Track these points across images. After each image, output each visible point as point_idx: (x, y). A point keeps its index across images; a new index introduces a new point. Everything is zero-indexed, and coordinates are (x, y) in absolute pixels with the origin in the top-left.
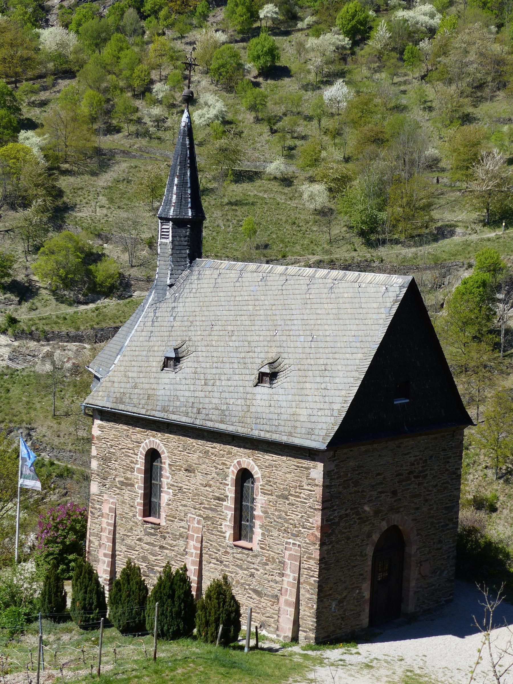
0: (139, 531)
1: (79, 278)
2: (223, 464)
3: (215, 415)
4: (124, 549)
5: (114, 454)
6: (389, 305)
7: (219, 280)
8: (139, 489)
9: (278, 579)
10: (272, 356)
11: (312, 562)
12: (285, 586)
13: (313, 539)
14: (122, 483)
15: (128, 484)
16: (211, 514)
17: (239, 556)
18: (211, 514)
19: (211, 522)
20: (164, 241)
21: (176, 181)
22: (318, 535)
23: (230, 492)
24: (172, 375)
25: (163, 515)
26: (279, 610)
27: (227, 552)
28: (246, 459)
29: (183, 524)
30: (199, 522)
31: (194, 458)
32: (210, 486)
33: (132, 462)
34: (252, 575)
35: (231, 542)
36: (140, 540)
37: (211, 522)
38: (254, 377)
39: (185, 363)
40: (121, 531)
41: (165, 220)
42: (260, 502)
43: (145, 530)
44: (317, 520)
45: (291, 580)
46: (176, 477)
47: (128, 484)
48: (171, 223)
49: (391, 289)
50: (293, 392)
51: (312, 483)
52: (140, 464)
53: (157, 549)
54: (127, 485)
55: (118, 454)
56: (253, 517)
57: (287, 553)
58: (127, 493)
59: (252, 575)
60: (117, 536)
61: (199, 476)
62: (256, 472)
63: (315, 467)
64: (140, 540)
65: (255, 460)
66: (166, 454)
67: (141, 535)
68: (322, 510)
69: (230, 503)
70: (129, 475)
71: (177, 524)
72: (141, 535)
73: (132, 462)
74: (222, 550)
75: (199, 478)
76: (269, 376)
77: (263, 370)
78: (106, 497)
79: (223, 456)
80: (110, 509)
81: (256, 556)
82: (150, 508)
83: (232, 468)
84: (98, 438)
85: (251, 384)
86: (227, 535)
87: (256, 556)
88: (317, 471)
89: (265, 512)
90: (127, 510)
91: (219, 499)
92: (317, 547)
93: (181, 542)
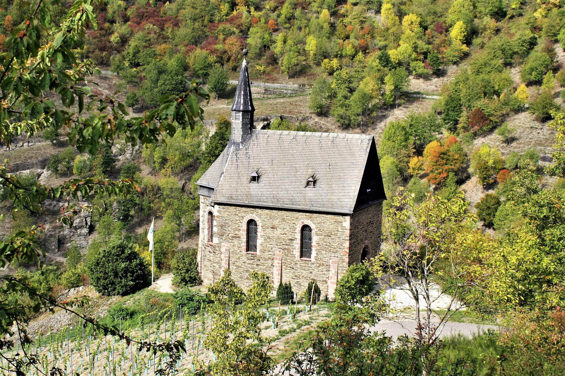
0: (244, 259)
1: (102, 140)
2: (294, 223)
3: (287, 201)
4: (235, 267)
5: (227, 223)
6: (365, 148)
7: (269, 139)
8: (244, 238)
9: (326, 273)
10: (310, 172)
11: (344, 264)
12: (330, 275)
13: (345, 253)
14: (233, 237)
15: (237, 237)
16: (286, 247)
17: (303, 265)
18: (286, 247)
19: (287, 251)
20: (237, 121)
21: (242, 93)
22: (348, 251)
23: (298, 236)
24: (257, 184)
25: (258, 249)
26: (328, 286)
27: (296, 264)
28: (305, 219)
29: (270, 253)
30: (280, 251)
31: (276, 222)
32: (286, 234)
33: (239, 226)
34: (311, 273)
35: (299, 259)
36: (244, 263)
37: (287, 251)
38: (305, 182)
39: (261, 179)
40: (233, 260)
41: (239, 111)
42: (315, 239)
43: (247, 258)
44: (347, 244)
45: (334, 272)
46: (266, 232)
47: (237, 237)
48: (241, 113)
49: (364, 141)
50: (326, 189)
51: (344, 228)
52: (244, 227)
53: (255, 266)
54: (236, 237)
55: (230, 223)
56: (311, 246)
57: (331, 261)
58: (236, 241)
59: (311, 273)
60: (230, 262)
61: (279, 230)
62: (312, 226)
63: (345, 221)
64: (244, 263)
65: (311, 221)
66: (260, 221)
67: (245, 260)
68: (350, 240)
69: (298, 241)
70: (237, 232)
71: (266, 253)
72: (245, 260)
73: (239, 226)
74: (293, 263)
75: (278, 232)
76: (313, 182)
77: (309, 180)
78: (223, 244)
79: (293, 220)
80: (226, 250)
81: (313, 264)
82: (250, 246)
83: (298, 225)
84: (217, 217)
85: (303, 186)
86: (296, 256)
87: (313, 264)
88: (347, 222)
89: (318, 244)
90: (236, 248)
91: (291, 240)
92: (347, 256)
93: (269, 261)
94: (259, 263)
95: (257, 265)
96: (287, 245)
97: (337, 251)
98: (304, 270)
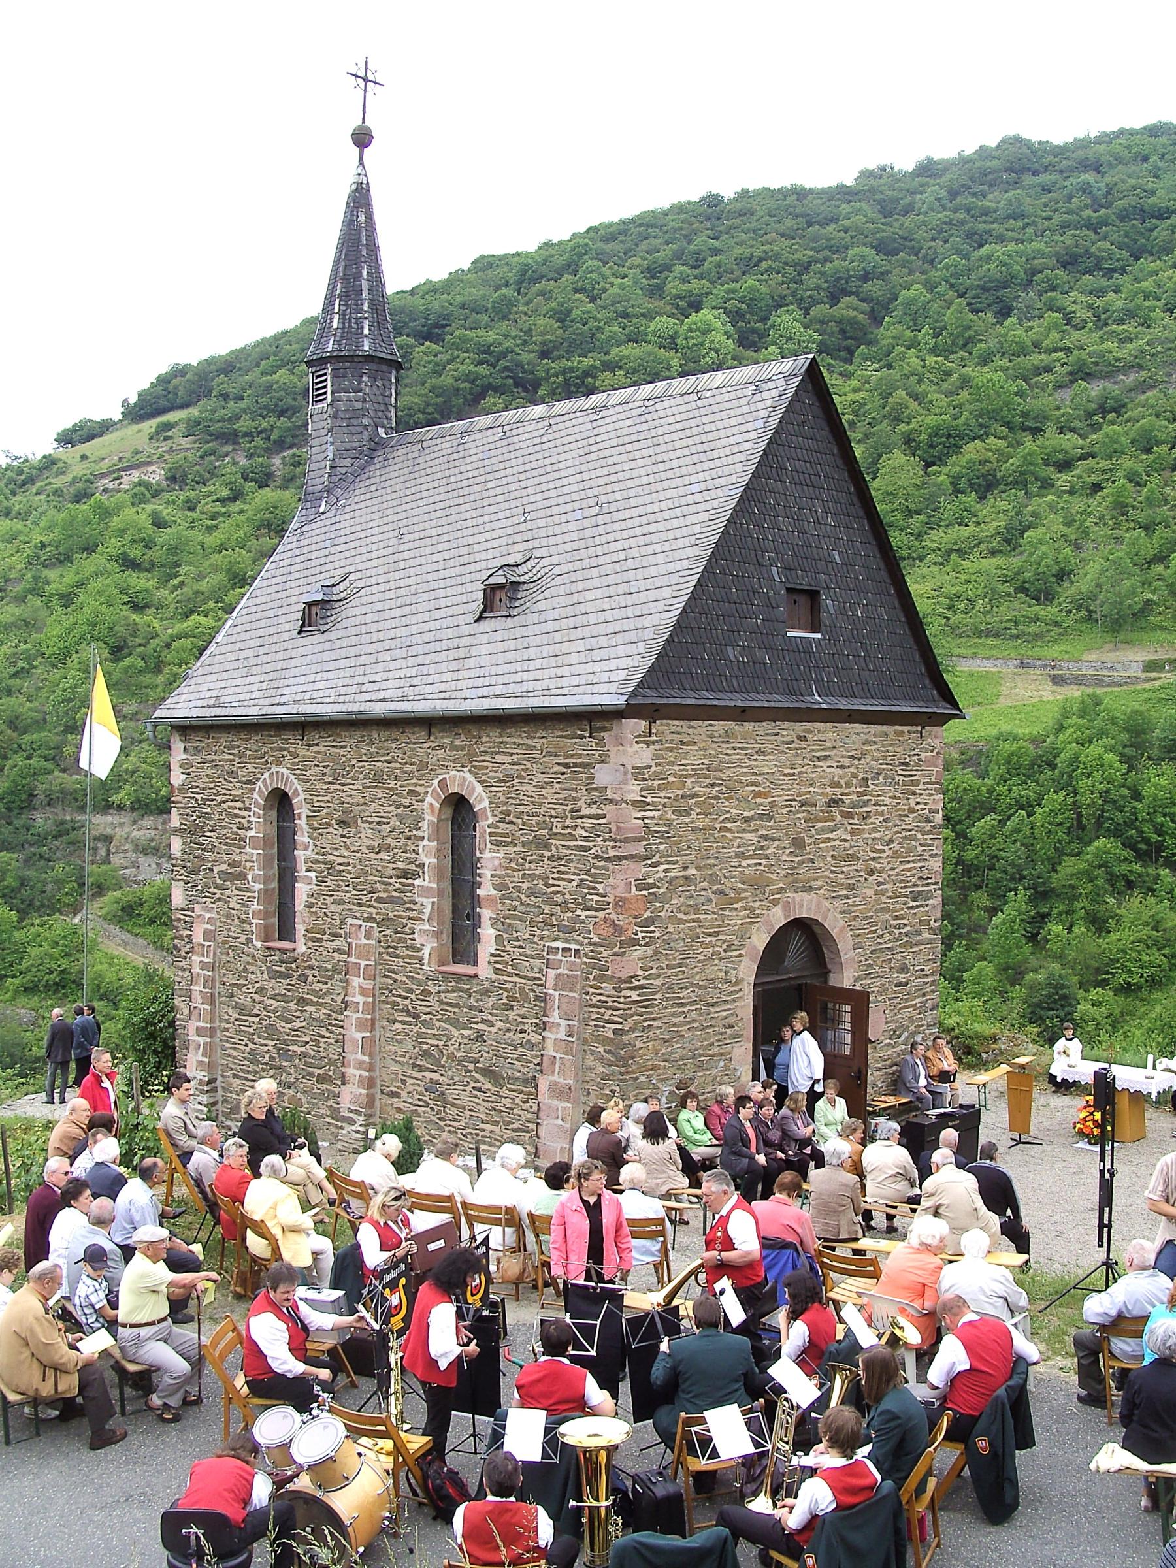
2: (412, 793)
12: (550, 1051)
16: (390, 911)
23: (429, 853)
27: (426, 993)
30: (368, 936)
31: (353, 794)
32: (387, 850)
34: (480, 1038)
36: (260, 991)
57: (552, 973)
59: (480, 1038)
66: (302, 796)
75: (365, 836)
79: (410, 775)
81: (486, 992)
91: (405, 874)
94: (303, 991)
95: (301, 1001)
96: (392, 901)
97: (577, 919)
98: (456, 1023)
